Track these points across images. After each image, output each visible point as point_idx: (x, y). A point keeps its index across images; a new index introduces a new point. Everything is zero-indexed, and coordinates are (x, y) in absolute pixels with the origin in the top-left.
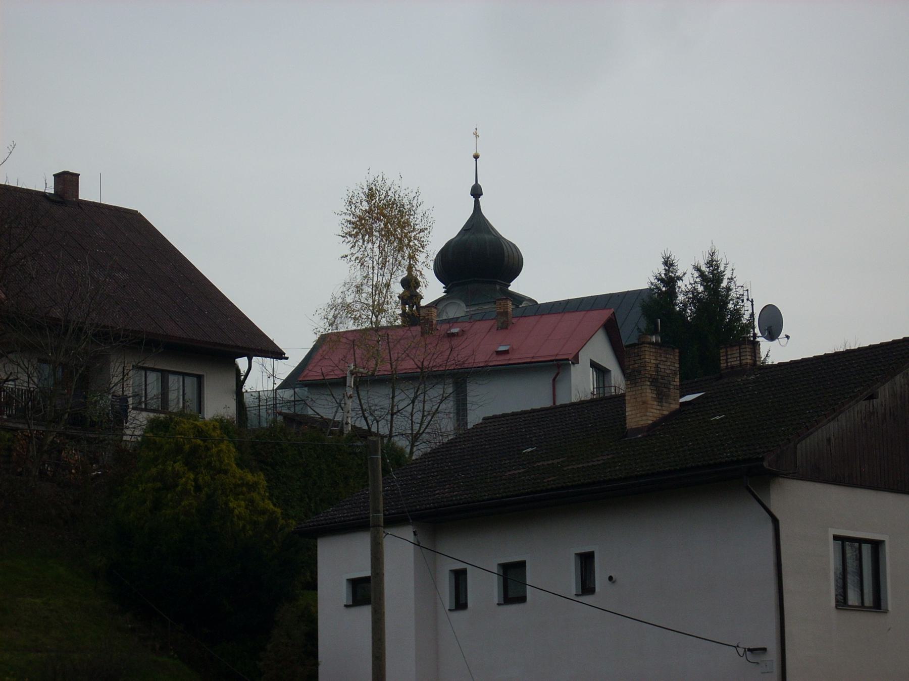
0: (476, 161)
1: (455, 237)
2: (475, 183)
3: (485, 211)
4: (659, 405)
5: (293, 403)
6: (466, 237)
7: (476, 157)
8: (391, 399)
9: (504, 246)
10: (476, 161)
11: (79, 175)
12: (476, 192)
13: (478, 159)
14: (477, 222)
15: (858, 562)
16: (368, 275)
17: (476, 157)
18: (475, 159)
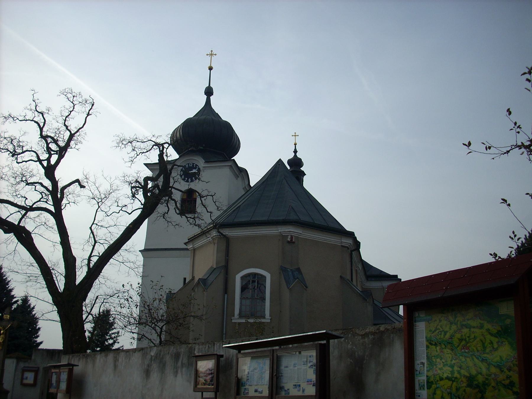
7: (211, 69)
13: (211, 71)
17: (211, 69)
18: (209, 71)
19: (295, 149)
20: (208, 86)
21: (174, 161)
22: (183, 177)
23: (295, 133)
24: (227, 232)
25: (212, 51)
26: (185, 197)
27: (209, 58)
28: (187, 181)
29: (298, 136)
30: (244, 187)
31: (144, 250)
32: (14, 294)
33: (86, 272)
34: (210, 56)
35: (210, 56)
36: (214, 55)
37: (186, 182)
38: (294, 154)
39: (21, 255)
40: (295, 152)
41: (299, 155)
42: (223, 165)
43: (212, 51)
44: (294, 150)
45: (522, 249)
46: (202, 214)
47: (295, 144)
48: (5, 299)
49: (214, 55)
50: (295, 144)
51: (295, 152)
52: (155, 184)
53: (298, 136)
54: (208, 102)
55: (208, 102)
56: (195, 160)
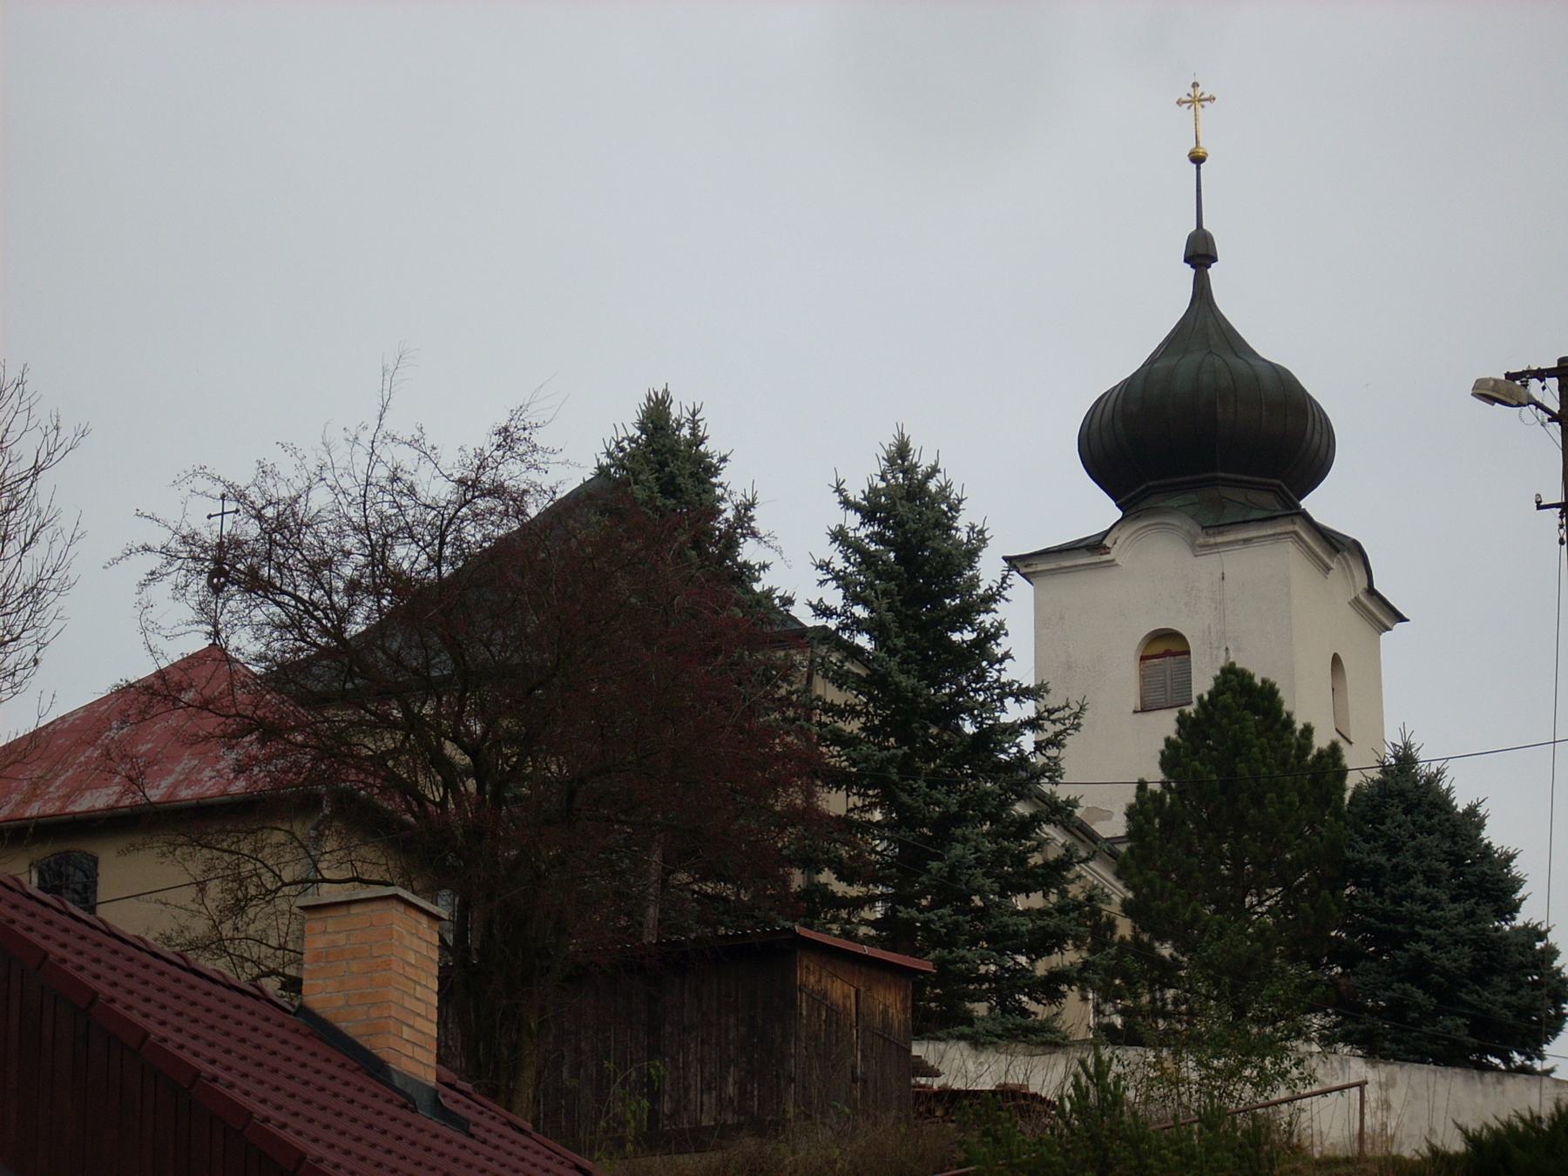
7: (1197, 159)
17: (1197, 159)
20: (1195, 228)
21: (1100, 538)
27: (1186, 113)
30: (1353, 597)
32: (1560, 966)
34: (1193, 108)
35: (1189, 108)
36: (1185, 102)
39: (404, 1042)
45: (868, 780)
48: (1536, 978)
49: (1185, 102)
52: (217, 654)
54: (1202, 291)
55: (1202, 291)
56: (1173, 525)
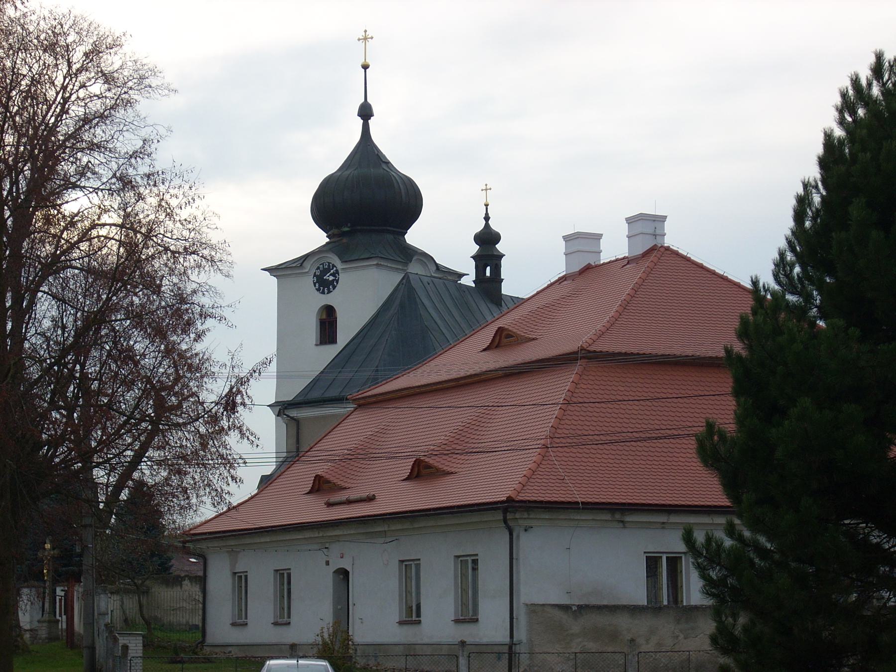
0: (365, 72)
1: (336, 172)
2: (363, 100)
3: (377, 137)
4: (329, 635)
5: (688, 653)
6: (348, 172)
7: (365, 67)
8: (185, 666)
9: (394, 181)
10: (365, 72)
11: (663, 219)
12: (366, 112)
13: (367, 70)
14: (366, 147)
15: (494, 369)
16: (80, 88)
17: (365, 67)
18: (363, 70)
19: (487, 214)
22: (317, 285)
23: (486, 185)
24: (294, 413)
25: (366, 31)
26: (324, 317)
28: (323, 293)
29: (490, 189)
31: (275, 405)
33: (819, 158)
37: (322, 293)
38: (484, 222)
40: (487, 218)
41: (494, 225)
42: (365, 264)
43: (366, 31)
44: (484, 216)
46: (850, 75)
47: (487, 205)
50: (487, 205)
51: (487, 218)
53: (490, 189)
